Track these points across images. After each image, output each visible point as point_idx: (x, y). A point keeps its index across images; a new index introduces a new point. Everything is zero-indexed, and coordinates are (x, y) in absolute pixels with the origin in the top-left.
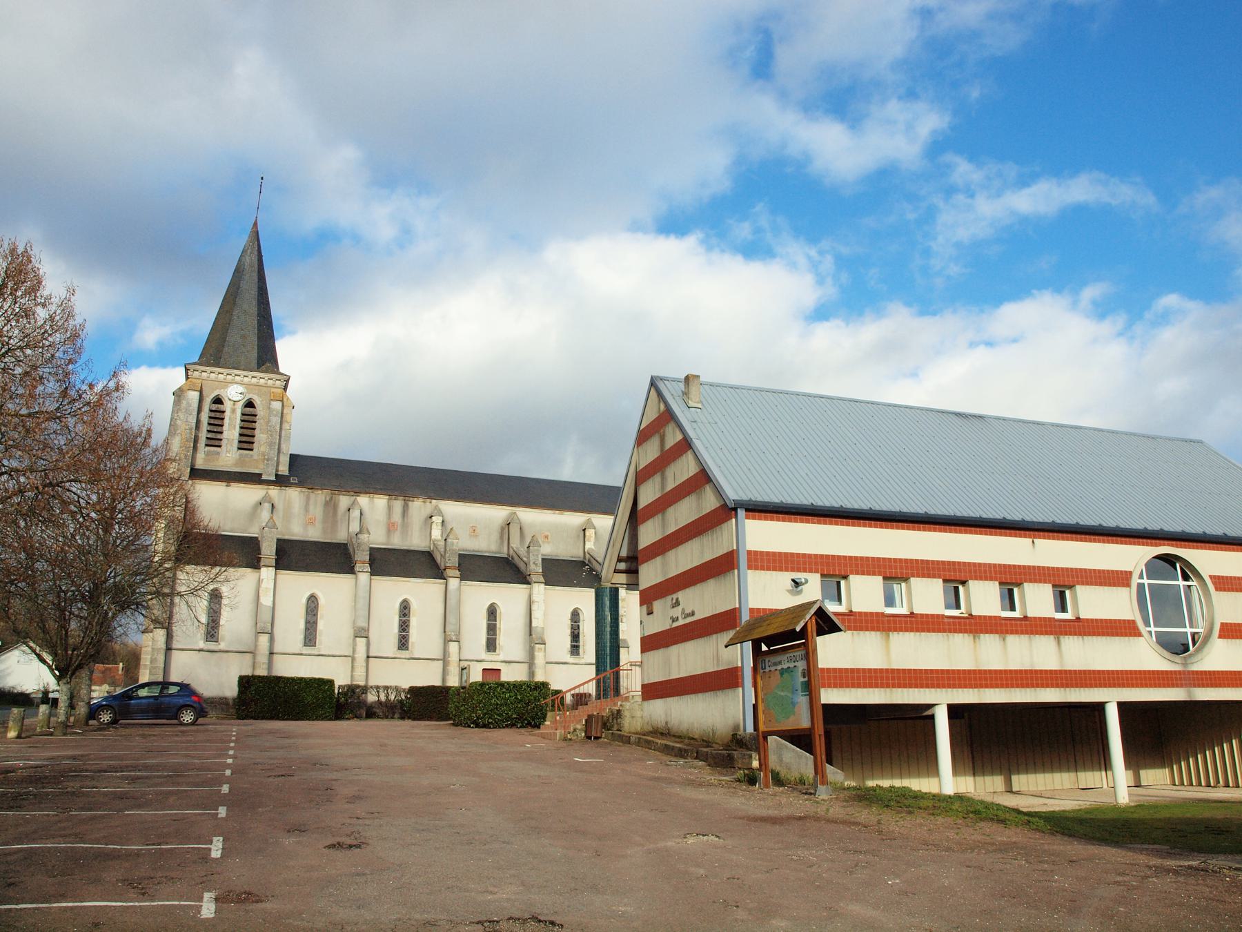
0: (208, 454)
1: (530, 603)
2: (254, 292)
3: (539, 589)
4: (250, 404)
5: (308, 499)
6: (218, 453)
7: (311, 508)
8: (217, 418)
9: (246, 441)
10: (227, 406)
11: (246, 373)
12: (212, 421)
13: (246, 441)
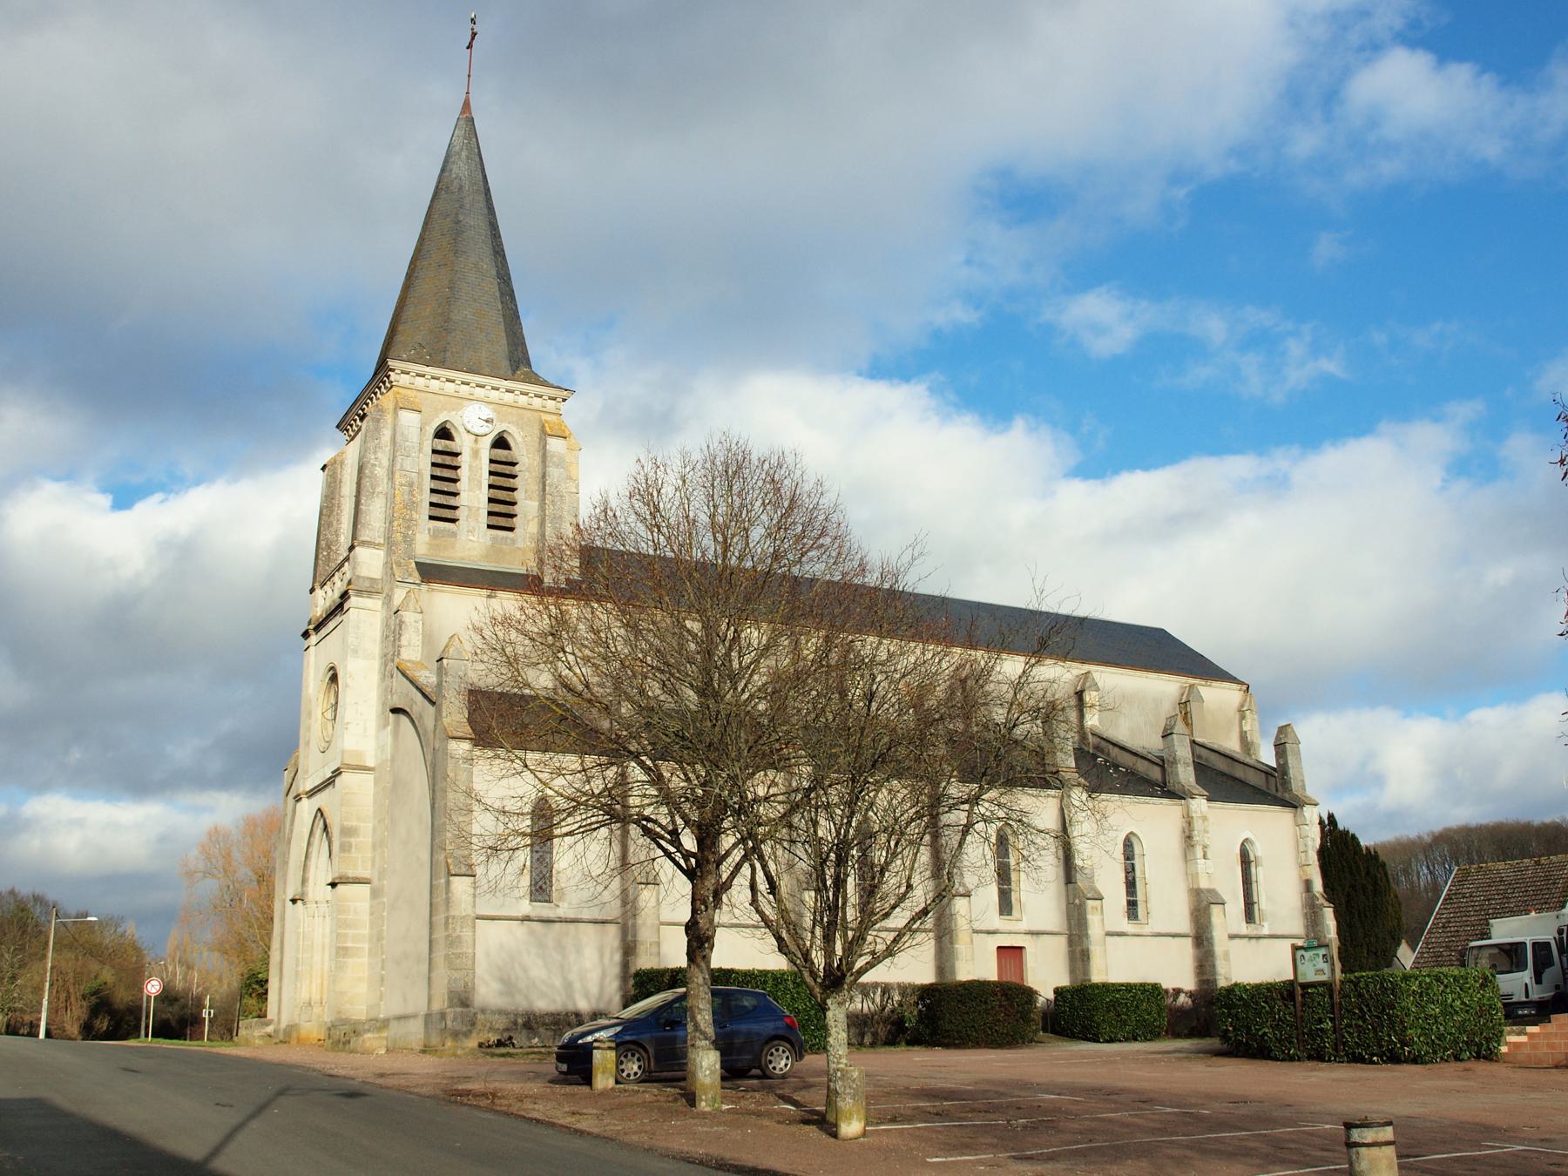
0: (435, 535)
1: (1189, 821)
2: (484, 229)
4: (501, 443)
6: (454, 535)
8: (445, 467)
9: (502, 515)
10: (462, 443)
12: (439, 472)
13: (502, 515)
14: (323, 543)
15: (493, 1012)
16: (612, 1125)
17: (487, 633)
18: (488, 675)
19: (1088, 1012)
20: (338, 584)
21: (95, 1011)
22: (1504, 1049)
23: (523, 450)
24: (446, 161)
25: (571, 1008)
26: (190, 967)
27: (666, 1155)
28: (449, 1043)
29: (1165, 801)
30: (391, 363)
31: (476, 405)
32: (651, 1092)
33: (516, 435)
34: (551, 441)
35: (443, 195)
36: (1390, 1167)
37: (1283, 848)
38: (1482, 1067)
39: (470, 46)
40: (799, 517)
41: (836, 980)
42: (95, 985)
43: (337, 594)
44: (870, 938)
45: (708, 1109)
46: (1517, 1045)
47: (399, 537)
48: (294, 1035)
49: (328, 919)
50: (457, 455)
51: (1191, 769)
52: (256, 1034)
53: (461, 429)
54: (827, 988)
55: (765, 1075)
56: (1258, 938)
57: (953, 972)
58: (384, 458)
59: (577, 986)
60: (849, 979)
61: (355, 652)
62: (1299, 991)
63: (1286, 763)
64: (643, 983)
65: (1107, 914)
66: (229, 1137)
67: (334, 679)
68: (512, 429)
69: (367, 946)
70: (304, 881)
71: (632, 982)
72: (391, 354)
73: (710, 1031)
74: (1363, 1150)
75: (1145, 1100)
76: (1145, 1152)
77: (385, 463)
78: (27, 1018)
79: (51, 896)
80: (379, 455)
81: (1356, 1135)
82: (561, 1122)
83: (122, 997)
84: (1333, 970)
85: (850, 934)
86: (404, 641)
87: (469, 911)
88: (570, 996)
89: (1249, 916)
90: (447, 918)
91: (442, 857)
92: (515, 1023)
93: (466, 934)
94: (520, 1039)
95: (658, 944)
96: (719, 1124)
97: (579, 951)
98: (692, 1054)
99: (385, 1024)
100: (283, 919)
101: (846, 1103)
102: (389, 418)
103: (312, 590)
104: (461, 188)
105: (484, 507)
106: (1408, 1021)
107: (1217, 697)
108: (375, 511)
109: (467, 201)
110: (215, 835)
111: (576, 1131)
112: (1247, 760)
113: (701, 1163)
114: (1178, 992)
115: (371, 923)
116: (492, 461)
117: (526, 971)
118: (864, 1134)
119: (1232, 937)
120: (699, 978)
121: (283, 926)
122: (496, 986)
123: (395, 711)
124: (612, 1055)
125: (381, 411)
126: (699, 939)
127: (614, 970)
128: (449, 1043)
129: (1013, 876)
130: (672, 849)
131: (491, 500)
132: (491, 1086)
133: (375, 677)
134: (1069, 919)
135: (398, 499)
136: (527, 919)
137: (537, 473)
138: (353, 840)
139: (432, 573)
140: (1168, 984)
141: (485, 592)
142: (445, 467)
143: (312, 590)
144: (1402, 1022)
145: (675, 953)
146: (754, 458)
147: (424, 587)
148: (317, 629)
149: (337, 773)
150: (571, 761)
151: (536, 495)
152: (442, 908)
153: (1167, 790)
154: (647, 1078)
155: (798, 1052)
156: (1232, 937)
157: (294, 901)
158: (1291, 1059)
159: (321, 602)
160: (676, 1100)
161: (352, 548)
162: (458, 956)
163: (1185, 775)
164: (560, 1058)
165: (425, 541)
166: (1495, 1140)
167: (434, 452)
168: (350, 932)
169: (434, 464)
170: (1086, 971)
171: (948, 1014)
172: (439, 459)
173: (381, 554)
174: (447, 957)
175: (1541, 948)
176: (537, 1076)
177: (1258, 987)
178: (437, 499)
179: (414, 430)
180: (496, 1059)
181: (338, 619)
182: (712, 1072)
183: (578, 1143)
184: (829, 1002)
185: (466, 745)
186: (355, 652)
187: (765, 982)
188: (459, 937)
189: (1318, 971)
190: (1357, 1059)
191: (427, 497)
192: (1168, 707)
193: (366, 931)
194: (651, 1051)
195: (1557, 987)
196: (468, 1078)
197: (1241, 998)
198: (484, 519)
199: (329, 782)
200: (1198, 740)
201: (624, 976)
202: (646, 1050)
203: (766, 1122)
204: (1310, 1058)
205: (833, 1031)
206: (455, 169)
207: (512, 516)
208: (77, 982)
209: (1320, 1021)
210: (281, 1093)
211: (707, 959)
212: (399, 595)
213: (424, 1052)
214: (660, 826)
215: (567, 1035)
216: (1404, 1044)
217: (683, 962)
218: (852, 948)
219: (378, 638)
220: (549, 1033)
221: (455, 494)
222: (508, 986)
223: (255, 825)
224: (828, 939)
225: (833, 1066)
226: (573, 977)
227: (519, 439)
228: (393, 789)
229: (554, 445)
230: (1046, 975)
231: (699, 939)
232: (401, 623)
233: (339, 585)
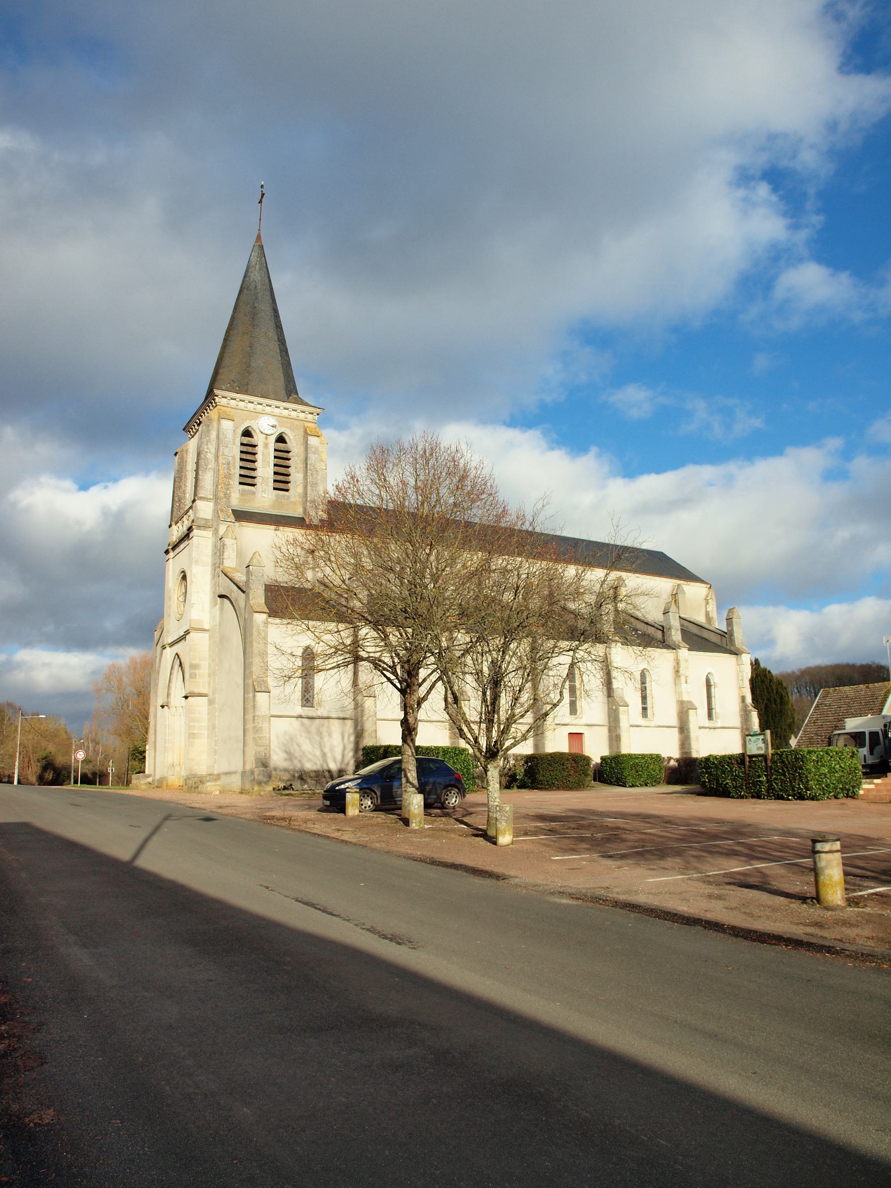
0: (243, 493)
1: (678, 662)
2: (270, 312)
4: (281, 439)
6: (254, 493)
8: (248, 454)
9: (282, 482)
10: (258, 439)
11: (278, 403)
12: (245, 456)
13: (282, 482)
14: (176, 498)
15: (281, 770)
16: (362, 837)
17: (284, 550)
18: (283, 577)
19: (614, 771)
20: (186, 522)
21: (45, 768)
22: (861, 792)
23: (294, 443)
24: (247, 271)
25: (325, 767)
26: (97, 743)
27: (399, 856)
28: (256, 788)
29: (665, 650)
30: (216, 391)
31: (266, 417)
32: (381, 817)
33: (290, 435)
34: (310, 438)
35: (245, 292)
36: (838, 865)
37: (731, 678)
38: (849, 801)
39: (260, 202)
40: (468, 482)
41: (492, 753)
42: (44, 754)
43: (185, 529)
44: (512, 730)
45: (417, 828)
46: (869, 790)
47: (221, 495)
48: (164, 783)
49: (183, 717)
50: (255, 446)
51: (679, 632)
52: (142, 782)
53: (258, 431)
54: (488, 758)
55: (443, 807)
57: (544, 747)
58: (212, 448)
59: (329, 755)
60: (501, 753)
61: (197, 562)
62: (747, 759)
63: (732, 630)
64: (370, 754)
65: (630, 715)
66: (142, 847)
67: (184, 578)
68: (287, 431)
69: (206, 732)
70: (168, 695)
71: (361, 753)
72: (216, 385)
73: (415, 782)
74: (823, 855)
75: (666, 821)
76: (678, 853)
77: (213, 451)
78: (7, 773)
79: (18, 704)
80: (209, 446)
81: (819, 847)
82: (332, 835)
83: (60, 760)
84: (767, 748)
85: (502, 727)
86: (225, 556)
87: (267, 713)
88: (325, 761)
89: (710, 716)
90: (254, 717)
91: (250, 681)
92: (294, 776)
93: (265, 725)
94: (297, 785)
95: (376, 731)
96: (425, 837)
97: (330, 735)
98: (405, 796)
99: (218, 777)
100: (155, 716)
101: (502, 825)
102: (215, 424)
103: (170, 526)
104: (256, 288)
105: (271, 477)
106: (810, 777)
107: (694, 592)
108: (208, 480)
109: (259, 295)
110: (113, 669)
111: (343, 841)
112: (710, 628)
113: (421, 861)
114: (670, 759)
116: (275, 450)
117: (299, 746)
118: (513, 843)
119: (700, 728)
120: (409, 751)
121: (156, 721)
122: (283, 755)
123: (221, 596)
124: (357, 796)
125: (210, 420)
126: (408, 730)
127: (351, 746)
129: (578, 693)
130: (392, 677)
131: (275, 473)
132: (287, 814)
133: (208, 577)
134: (609, 720)
135: (221, 472)
136: (300, 717)
137: (302, 457)
138: (197, 671)
139: (241, 516)
140: (665, 755)
141: (273, 527)
142: (248, 454)
143: (170, 526)
144: (807, 777)
145: (391, 736)
146: (442, 446)
147: (237, 524)
148: (174, 549)
149: (187, 632)
150: (332, 626)
151: (302, 470)
152: (251, 711)
153: (664, 643)
154: (377, 809)
155: (462, 792)
156: (700, 728)
157: (163, 707)
158: (742, 797)
159: (175, 533)
160: (396, 822)
161: (194, 501)
162: (261, 738)
163: (676, 636)
164: (325, 797)
165: (237, 497)
166: (872, 845)
167: (242, 444)
169: (241, 452)
170: (618, 747)
171: (536, 773)
172: (245, 449)
173: (211, 505)
174: (254, 739)
175: (874, 735)
176: (310, 807)
177: (723, 757)
178: (244, 472)
179: (230, 431)
180: (284, 797)
181: (186, 543)
182: (419, 807)
183: (346, 849)
184: (489, 766)
185: (265, 616)
186: (197, 562)
187: (438, 753)
189: (759, 748)
190: (780, 798)
191: (238, 471)
192: (666, 597)
194: (379, 793)
195: (882, 757)
196: (270, 809)
197: (714, 763)
198: (271, 484)
199: (182, 638)
200: (682, 616)
201: (356, 750)
202: (375, 793)
203: (453, 836)
204: (753, 797)
205: (491, 783)
207: (288, 482)
208: (34, 752)
209: (759, 776)
210: (167, 818)
211: (413, 741)
212: (222, 529)
213: (241, 793)
214: (384, 663)
215: (330, 784)
216: (807, 789)
217: (399, 742)
218: (503, 732)
219: (210, 554)
220: (313, 782)
221: (254, 470)
222: (290, 756)
223: (136, 663)
224: (489, 730)
225: (491, 803)
226: (326, 750)
227: (292, 437)
228: (220, 643)
229: (312, 440)
230: (596, 750)
231: (408, 730)
233: (186, 523)
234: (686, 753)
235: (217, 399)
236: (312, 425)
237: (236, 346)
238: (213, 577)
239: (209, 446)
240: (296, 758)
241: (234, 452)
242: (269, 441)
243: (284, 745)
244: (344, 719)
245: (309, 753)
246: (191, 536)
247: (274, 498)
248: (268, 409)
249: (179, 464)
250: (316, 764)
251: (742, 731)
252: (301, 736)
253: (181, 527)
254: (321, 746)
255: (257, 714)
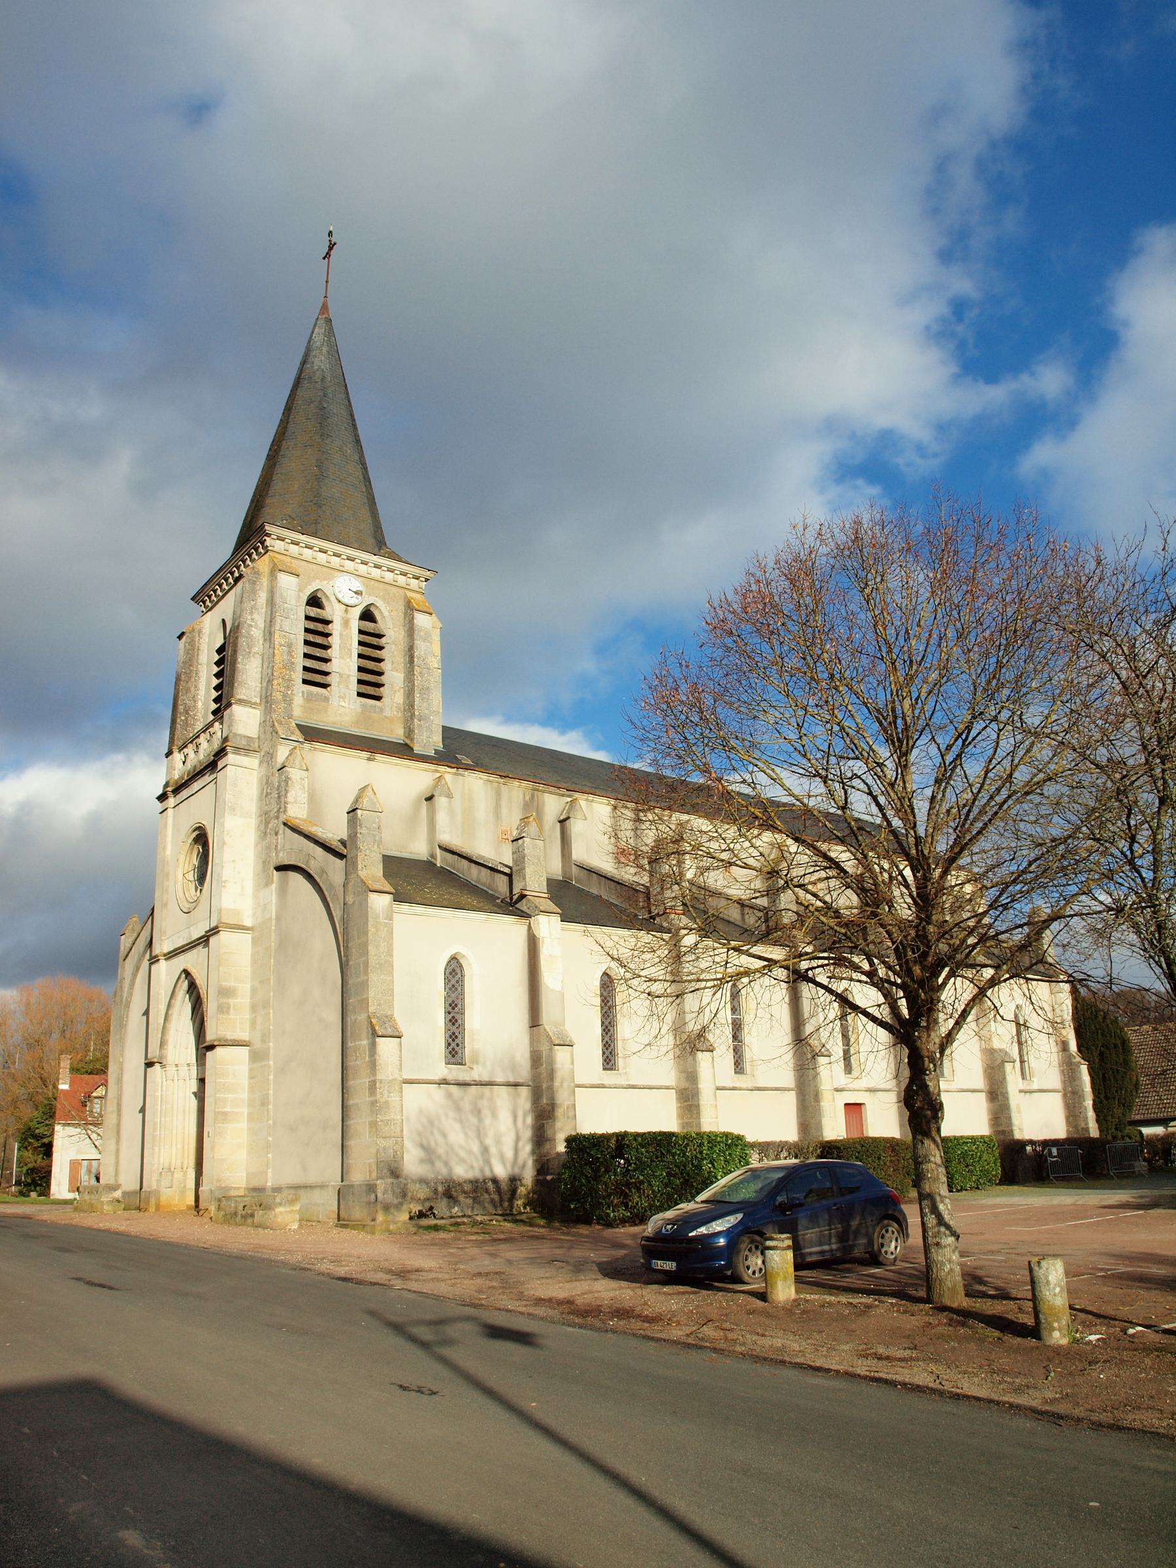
0: (308, 698)
3: (549, 926)
5: (498, 794)
6: (326, 699)
7: (504, 811)
8: (317, 633)
10: (332, 611)
13: (370, 684)
23: (390, 623)
25: (488, 1174)
31: (347, 577)
33: (383, 609)
34: (417, 615)
39: (327, 256)
45: (1064, 1341)
48: (153, 1201)
53: (333, 598)
56: (1031, 1092)
57: (819, 1127)
59: (493, 1150)
61: (233, 809)
68: (379, 603)
77: (261, 624)
80: (255, 616)
86: (290, 798)
87: (396, 1076)
88: (488, 1162)
92: (436, 1191)
93: (394, 1099)
94: (441, 1207)
97: (494, 1115)
102: (265, 581)
104: (324, 378)
105: (354, 675)
115: (252, 1089)
117: (444, 1135)
123: (280, 868)
125: (257, 573)
128: (380, 1217)
136: (445, 1082)
138: (231, 1001)
139: (312, 734)
141: (365, 755)
142: (317, 633)
147: (307, 746)
148: (177, 791)
149: (214, 931)
162: (387, 1122)
168: (229, 1096)
172: (311, 625)
179: (292, 593)
181: (207, 778)
183: (819, 1381)
185: (389, 898)
186: (233, 809)
188: (387, 1102)
191: (300, 662)
193: (245, 1095)
198: (354, 687)
199: (204, 940)
206: (317, 362)
207: (380, 685)
212: (282, 752)
226: (489, 1141)
227: (386, 614)
232: (287, 780)
234: (1004, 1132)
235: (268, 541)
236: (418, 596)
237: (293, 463)
238: (264, 835)
239: (255, 616)
240: (439, 1157)
241: (293, 628)
242: (350, 616)
243: (420, 1134)
244: (516, 1085)
245: (462, 1147)
246: (220, 764)
247: (359, 710)
248: (349, 565)
249: (187, 652)
250: (472, 1167)
251: (1065, 1095)
252: (447, 1116)
253: (192, 755)
254: (480, 1134)
255: (379, 1077)
